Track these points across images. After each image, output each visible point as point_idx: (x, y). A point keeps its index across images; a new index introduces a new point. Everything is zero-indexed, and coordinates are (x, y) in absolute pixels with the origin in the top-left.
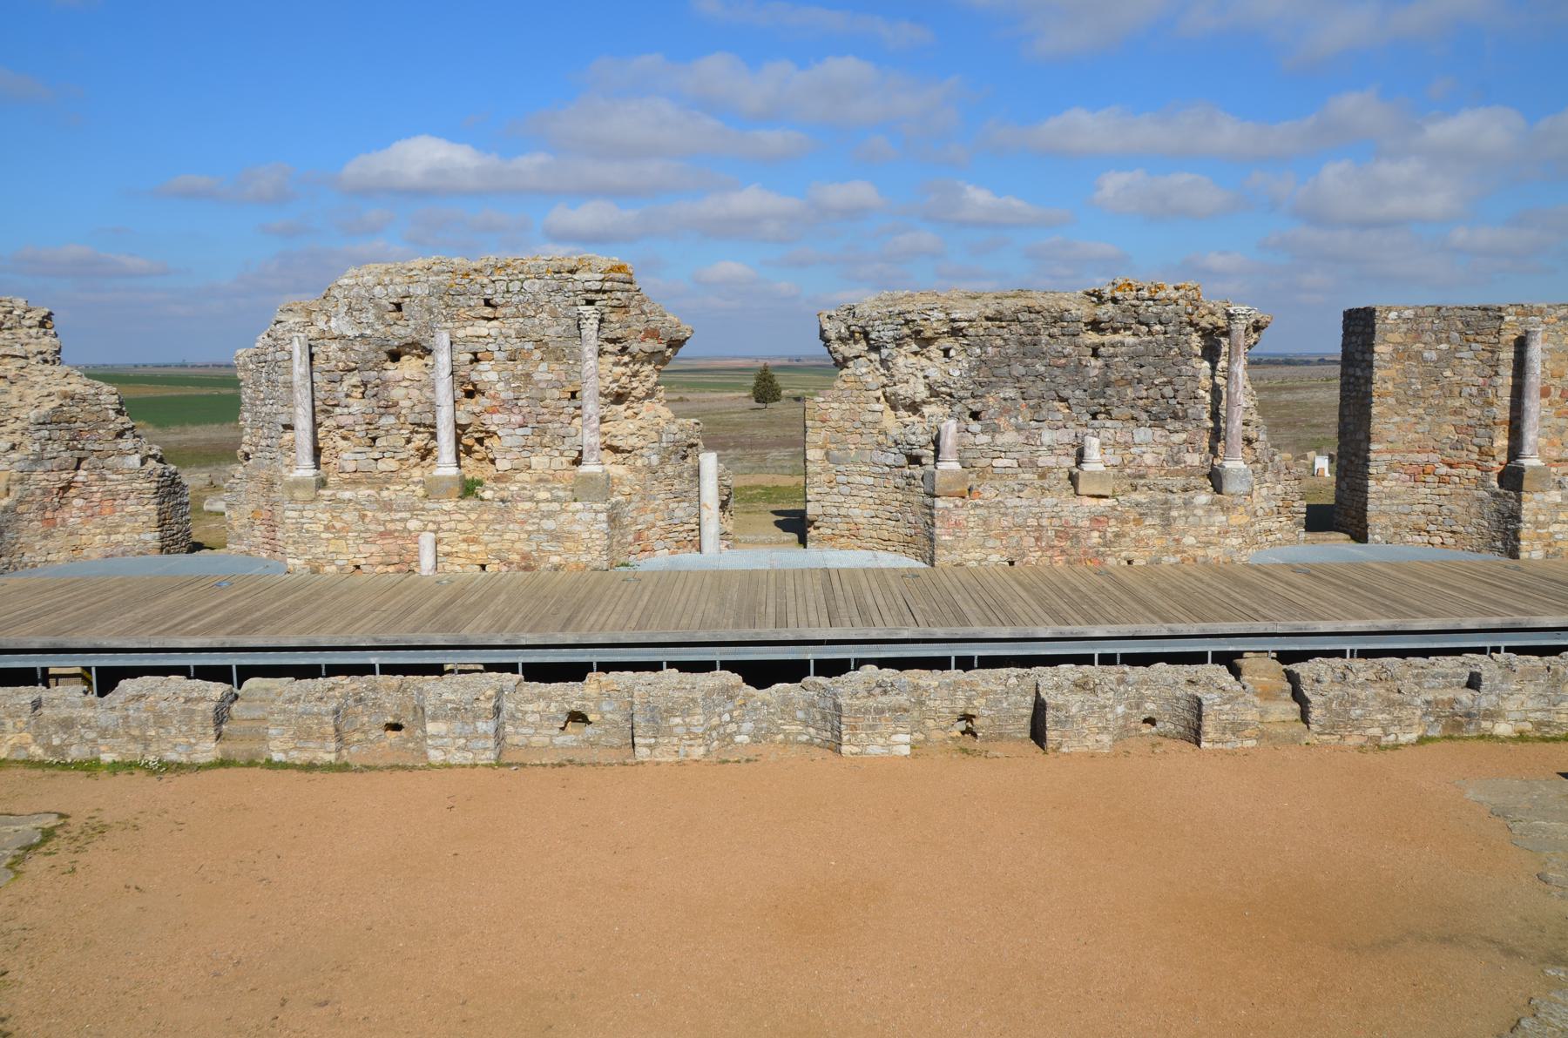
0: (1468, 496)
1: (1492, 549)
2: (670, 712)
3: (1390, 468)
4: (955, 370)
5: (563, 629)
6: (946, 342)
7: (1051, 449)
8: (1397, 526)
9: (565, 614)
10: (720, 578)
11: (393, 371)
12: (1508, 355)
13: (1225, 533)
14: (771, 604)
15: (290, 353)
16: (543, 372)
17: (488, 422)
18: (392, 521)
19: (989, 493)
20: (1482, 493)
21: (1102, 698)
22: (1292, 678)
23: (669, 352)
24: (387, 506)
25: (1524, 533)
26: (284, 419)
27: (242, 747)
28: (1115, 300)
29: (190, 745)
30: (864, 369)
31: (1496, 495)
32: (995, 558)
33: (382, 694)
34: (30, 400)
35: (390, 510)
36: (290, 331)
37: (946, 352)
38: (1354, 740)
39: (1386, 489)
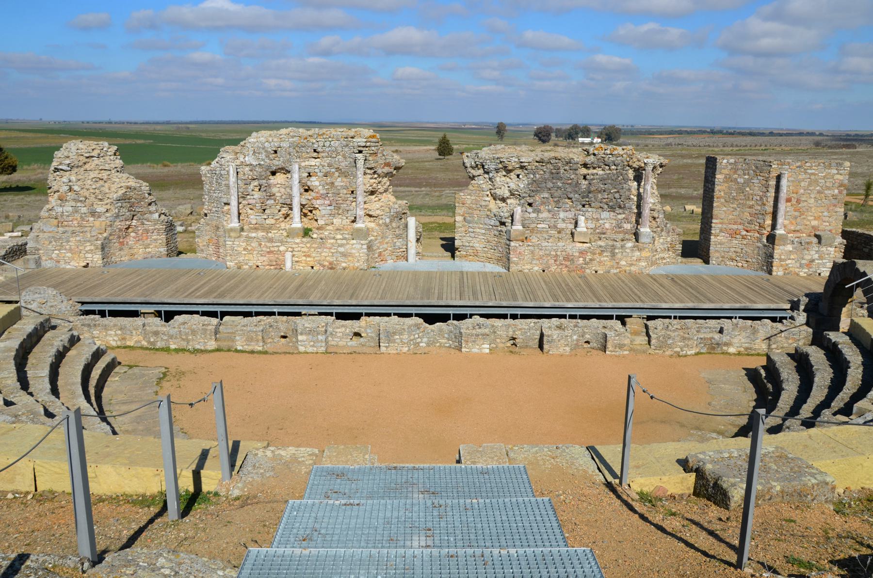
0: (755, 242)
2: (394, 333)
3: (721, 231)
4: (520, 184)
5: (351, 298)
6: (518, 172)
7: (563, 220)
8: (723, 257)
9: (351, 291)
10: (416, 275)
11: (273, 180)
12: (773, 183)
13: (639, 260)
14: (437, 289)
15: (228, 172)
16: (339, 182)
19: (534, 240)
20: (760, 245)
21: (566, 333)
22: (646, 327)
23: (395, 172)
24: (271, 240)
25: (775, 264)
26: (225, 201)
27: (225, 343)
28: (594, 155)
30: (482, 181)
31: (765, 246)
32: (536, 268)
33: (280, 324)
34: (113, 189)
37: (518, 176)
38: (669, 352)
39: (718, 240)
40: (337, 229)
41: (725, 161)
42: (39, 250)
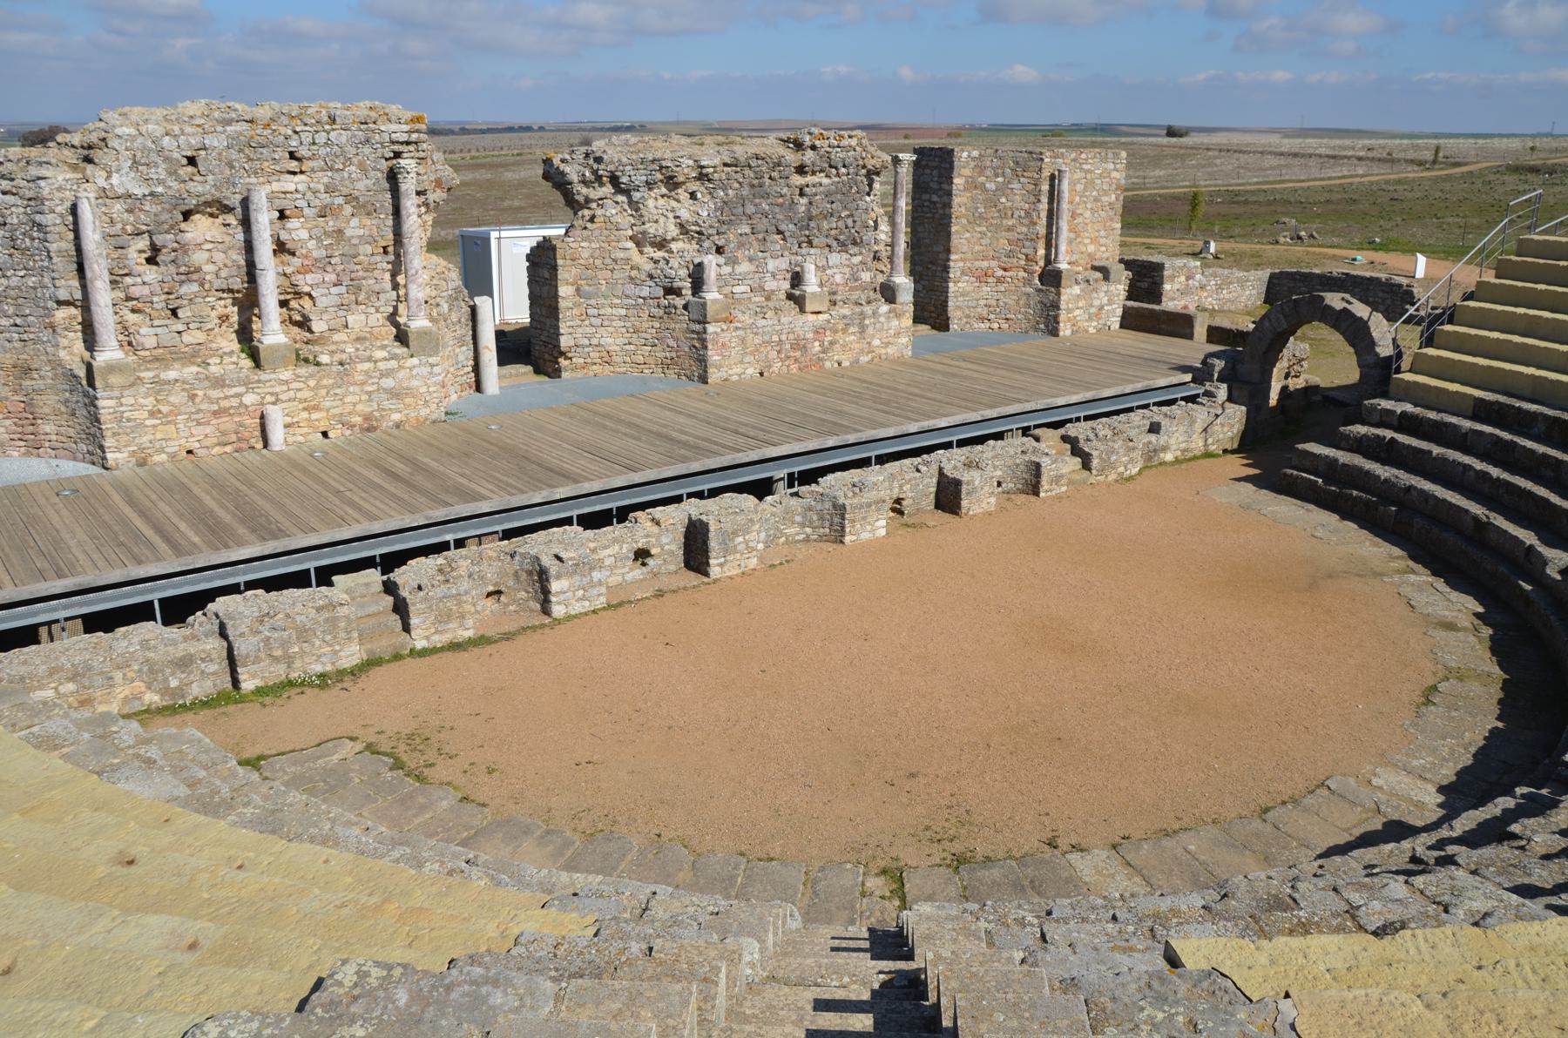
0: (1019, 290)
1: (1036, 330)
2: (735, 534)
3: (963, 273)
6: (693, 186)
8: (968, 316)
12: (1045, 187)
17: (301, 283)
18: (226, 397)
20: (1029, 290)
24: (219, 383)
27: (384, 642)
29: (335, 653)
32: (750, 371)
35: (223, 386)
36: (59, 189)
37: (693, 196)
40: (358, 339)
41: (965, 154)
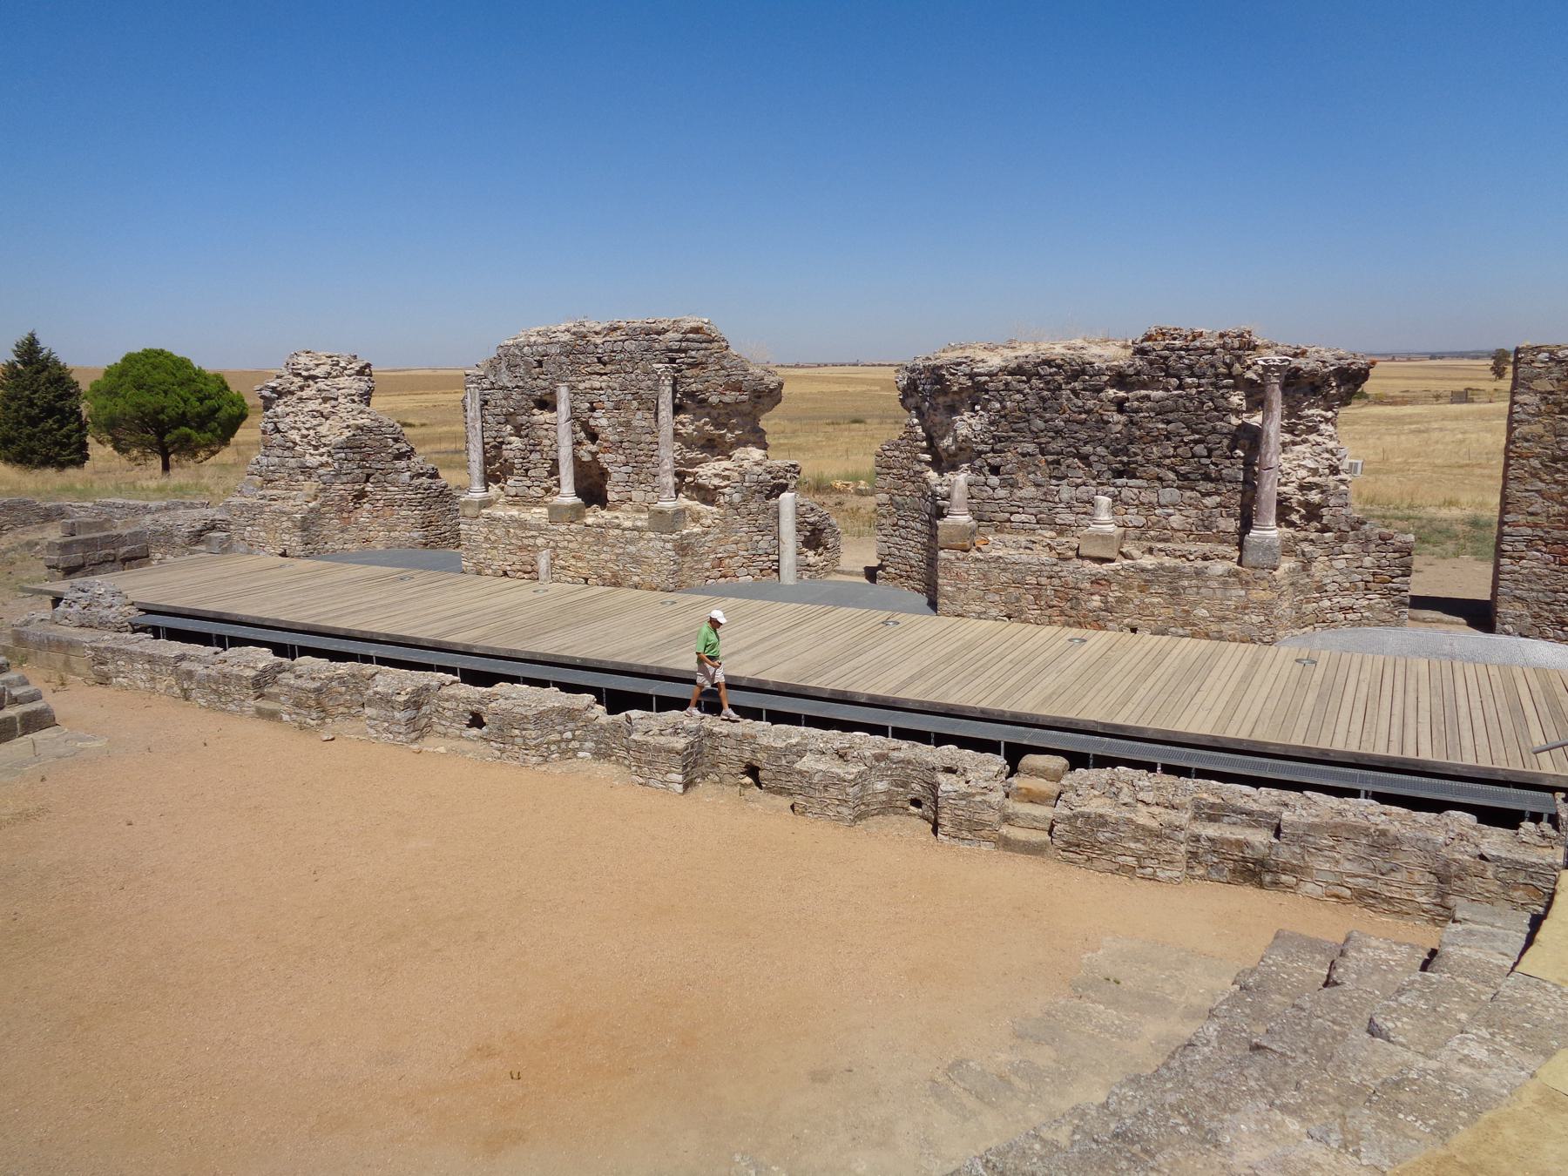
3: (1530, 544)
42: (229, 524)
